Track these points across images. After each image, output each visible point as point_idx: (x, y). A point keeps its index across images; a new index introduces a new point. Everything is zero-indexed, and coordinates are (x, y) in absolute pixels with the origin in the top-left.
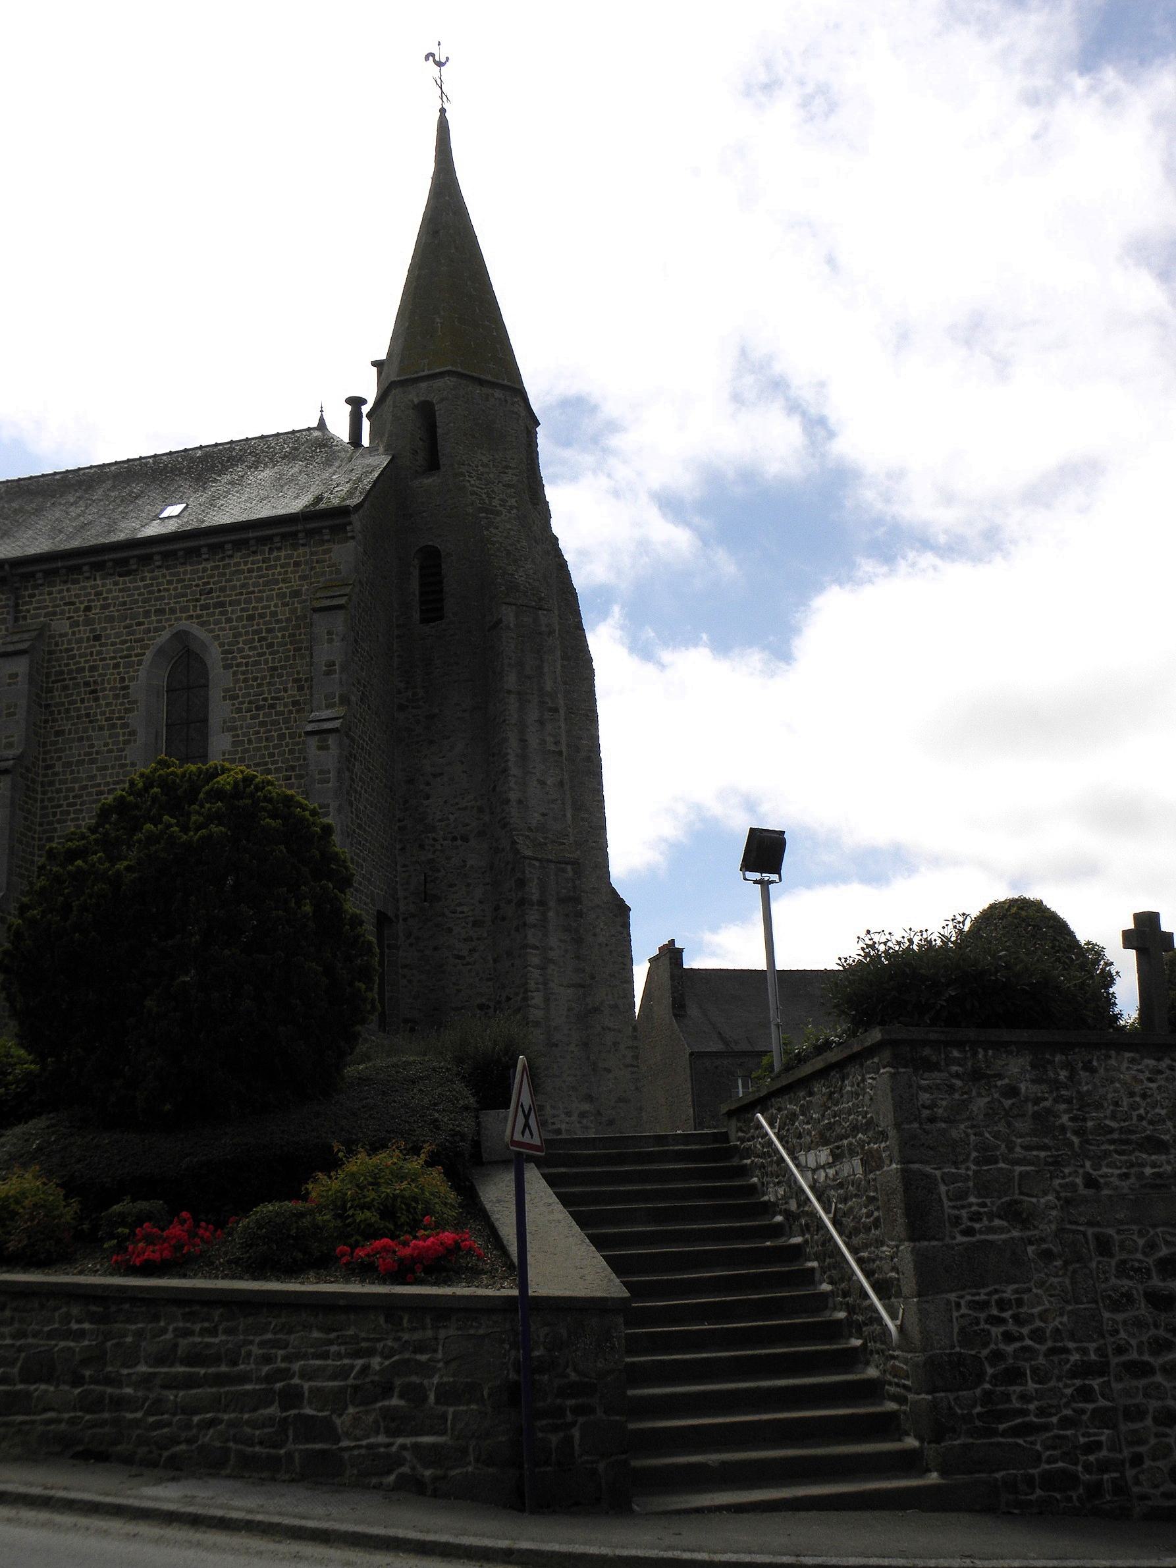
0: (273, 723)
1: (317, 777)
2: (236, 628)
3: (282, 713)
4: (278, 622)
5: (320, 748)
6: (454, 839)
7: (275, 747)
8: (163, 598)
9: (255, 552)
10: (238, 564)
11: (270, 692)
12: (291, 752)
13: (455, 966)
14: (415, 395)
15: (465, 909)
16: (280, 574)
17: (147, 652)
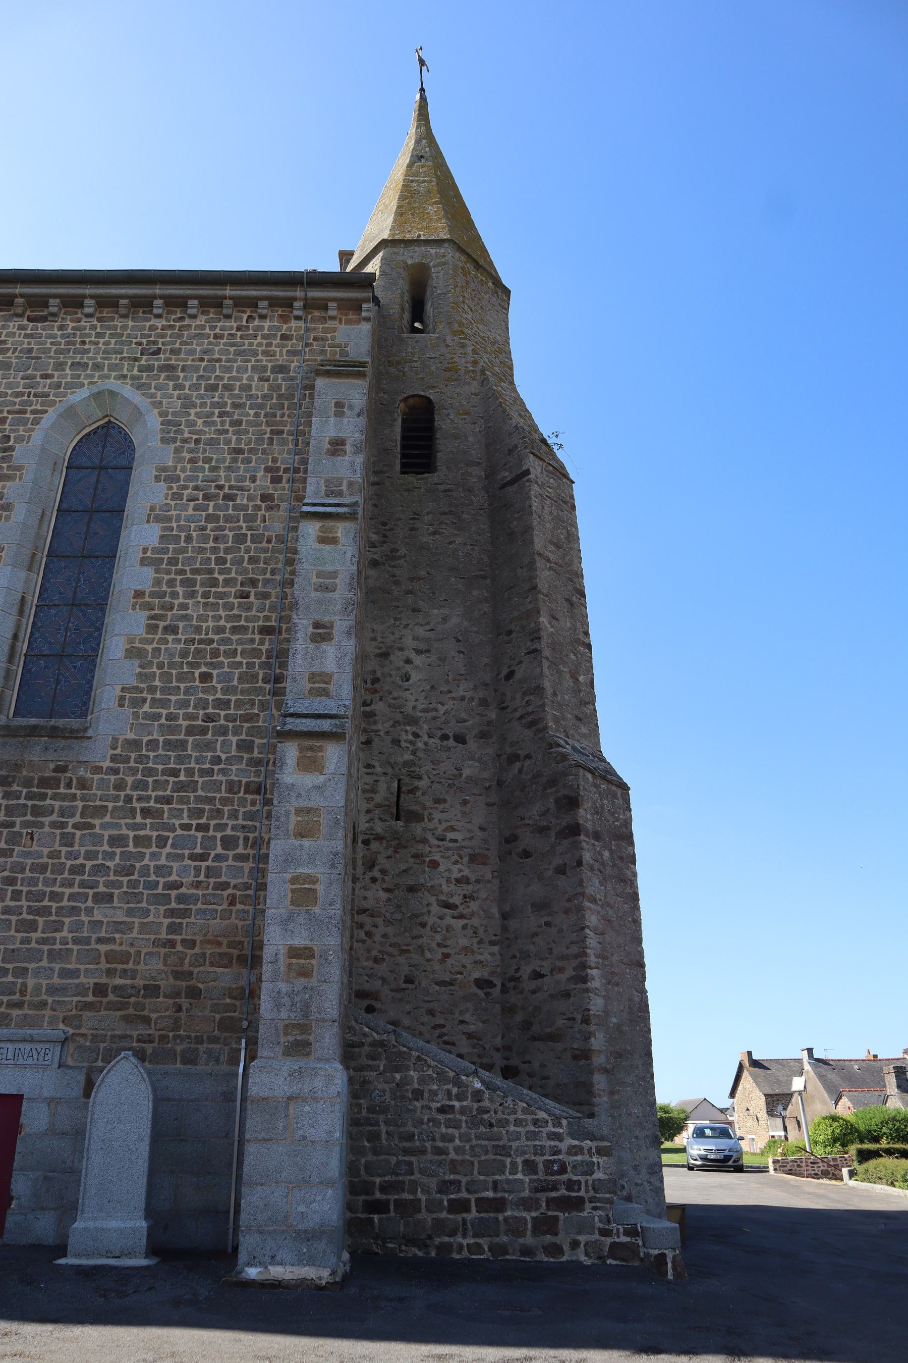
0: (228, 519)
1: (314, 580)
2: (187, 397)
3: (244, 508)
4: (250, 397)
5: (322, 540)
6: (445, 737)
7: (227, 550)
8: (87, 351)
9: (228, 317)
10: (203, 327)
11: (228, 479)
12: (253, 560)
13: (441, 918)
14: (411, 257)
15: (457, 836)
16: (260, 345)
17: (50, 410)
